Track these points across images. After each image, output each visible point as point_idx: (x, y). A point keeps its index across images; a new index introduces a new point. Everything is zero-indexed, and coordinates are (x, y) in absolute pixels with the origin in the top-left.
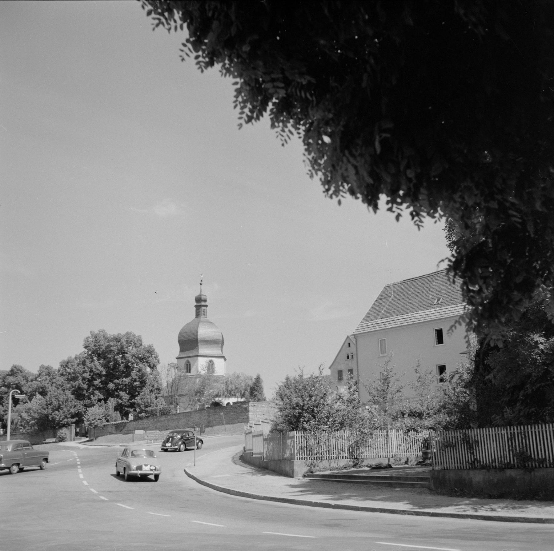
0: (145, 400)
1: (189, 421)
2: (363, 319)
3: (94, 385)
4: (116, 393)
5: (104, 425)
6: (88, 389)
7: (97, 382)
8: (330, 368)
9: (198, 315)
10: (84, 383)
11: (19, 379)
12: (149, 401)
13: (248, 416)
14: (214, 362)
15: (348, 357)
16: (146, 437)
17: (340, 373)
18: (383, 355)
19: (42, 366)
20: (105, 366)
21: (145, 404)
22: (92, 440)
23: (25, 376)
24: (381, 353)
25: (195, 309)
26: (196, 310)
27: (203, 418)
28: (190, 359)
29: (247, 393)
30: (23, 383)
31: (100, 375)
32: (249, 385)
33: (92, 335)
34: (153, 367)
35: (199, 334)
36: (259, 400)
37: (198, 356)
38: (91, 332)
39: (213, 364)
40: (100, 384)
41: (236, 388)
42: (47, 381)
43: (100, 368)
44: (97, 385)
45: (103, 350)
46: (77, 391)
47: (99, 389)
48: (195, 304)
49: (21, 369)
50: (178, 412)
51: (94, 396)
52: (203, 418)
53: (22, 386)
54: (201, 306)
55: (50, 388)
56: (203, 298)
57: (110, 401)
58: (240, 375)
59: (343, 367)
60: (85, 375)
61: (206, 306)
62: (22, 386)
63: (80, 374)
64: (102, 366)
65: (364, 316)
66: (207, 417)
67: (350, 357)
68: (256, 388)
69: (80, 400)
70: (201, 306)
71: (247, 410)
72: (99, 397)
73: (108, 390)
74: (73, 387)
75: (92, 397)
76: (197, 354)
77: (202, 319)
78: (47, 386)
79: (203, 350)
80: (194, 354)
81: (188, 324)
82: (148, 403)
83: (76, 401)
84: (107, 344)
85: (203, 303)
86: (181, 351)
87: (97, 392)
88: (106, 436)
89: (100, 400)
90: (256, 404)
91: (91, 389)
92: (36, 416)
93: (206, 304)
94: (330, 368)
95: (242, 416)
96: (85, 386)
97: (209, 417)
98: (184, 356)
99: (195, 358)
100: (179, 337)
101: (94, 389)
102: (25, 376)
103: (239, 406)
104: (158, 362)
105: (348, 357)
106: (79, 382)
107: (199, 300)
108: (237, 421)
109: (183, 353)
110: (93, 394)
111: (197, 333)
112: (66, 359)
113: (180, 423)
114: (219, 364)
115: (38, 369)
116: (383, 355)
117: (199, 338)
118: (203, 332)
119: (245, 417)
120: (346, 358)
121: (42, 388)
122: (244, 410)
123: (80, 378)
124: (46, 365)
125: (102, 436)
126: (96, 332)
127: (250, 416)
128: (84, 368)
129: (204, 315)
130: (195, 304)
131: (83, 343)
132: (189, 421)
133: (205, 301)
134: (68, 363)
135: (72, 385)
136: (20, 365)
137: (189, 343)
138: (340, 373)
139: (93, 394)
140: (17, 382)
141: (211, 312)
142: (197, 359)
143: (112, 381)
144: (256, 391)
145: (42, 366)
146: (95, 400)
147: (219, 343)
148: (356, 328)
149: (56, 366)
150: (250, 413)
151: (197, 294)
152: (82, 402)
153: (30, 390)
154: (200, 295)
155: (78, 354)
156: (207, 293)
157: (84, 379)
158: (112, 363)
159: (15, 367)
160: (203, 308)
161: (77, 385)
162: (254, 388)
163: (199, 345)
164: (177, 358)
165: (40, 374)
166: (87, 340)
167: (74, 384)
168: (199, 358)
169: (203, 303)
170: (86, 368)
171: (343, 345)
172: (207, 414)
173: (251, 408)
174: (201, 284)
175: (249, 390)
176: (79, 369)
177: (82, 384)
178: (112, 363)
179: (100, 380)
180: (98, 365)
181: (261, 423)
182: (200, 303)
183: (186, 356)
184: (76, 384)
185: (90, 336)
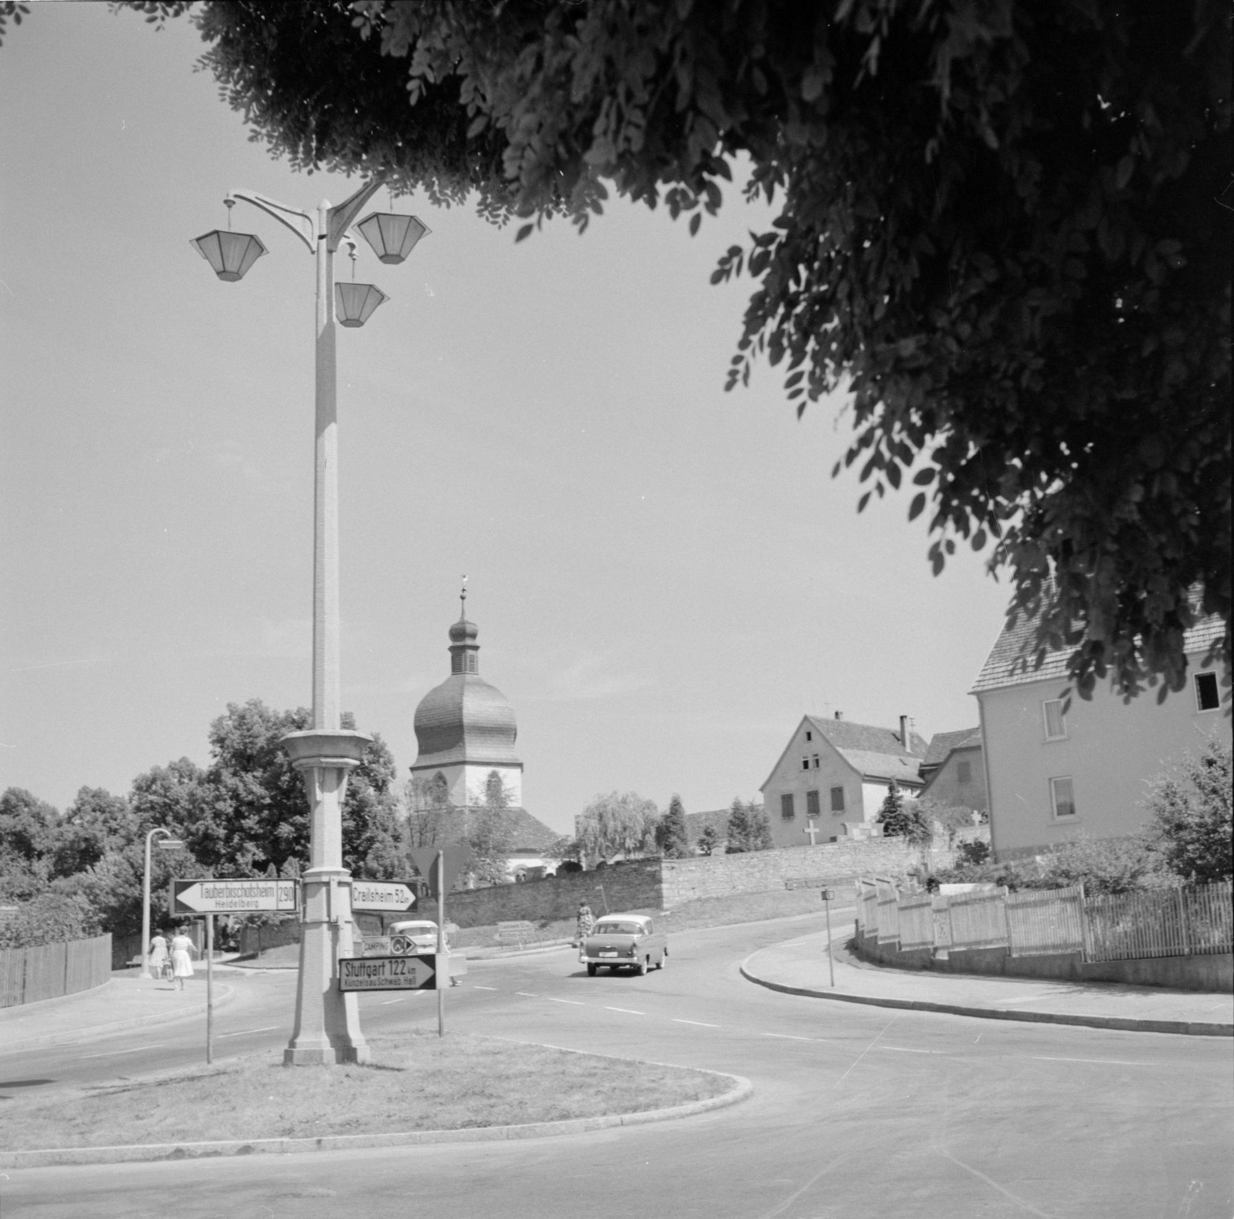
0: (388, 862)
1: (504, 906)
2: (991, 656)
3: (242, 829)
4: (298, 848)
5: (281, 922)
6: (228, 839)
7: (250, 822)
8: (762, 790)
9: (457, 667)
10: (218, 826)
11: (24, 820)
12: (396, 863)
13: (659, 891)
14: (501, 775)
15: (806, 764)
16: (497, 937)
17: (787, 800)
18: (1053, 738)
19: (85, 790)
20: (267, 784)
21: (385, 871)
22: (253, 957)
23: (39, 814)
24: (1051, 735)
25: (449, 654)
26: (453, 658)
27: (541, 899)
28: (444, 771)
29: (650, 839)
30: (34, 829)
31: (254, 806)
32: (653, 822)
33: (232, 713)
34: (380, 787)
35: (465, 711)
36: (681, 855)
37: (464, 763)
38: (229, 705)
39: (499, 781)
40: (256, 827)
41: (625, 829)
42: (99, 825)
43: (259, 790)
44: (251, 829)
45: (262, 748)
46: (199, 844)
47: (253, 837)
48: (450, 643)
49: (26, 798)
50: (471, 886)
51: (243, 855)
52: (541, 899)
53: (33, 836)
54: (464, 648)
55: (106, 840)
56: (469, 629)
57: (290, 864)
58: (631, 799)
59: (797, 785)
60: (220, 805)
61: (476, 648)
62: (33, 836)
63: (207, 803)
64: (261, 784)
65: (991, 648)
66: (551, 896)
67: (811, 764)
68: (673, 828)
69: (206, 864)
70: (464, 648)
71: (656, 879)
72: (256, 858)
73: (277, 840)
74: (192, 834)
75: (238, 856)
76: (461, 759)
77: (469, 677)
78: (99, 835)
79: (474, 748)
80: (454, 759)
81: (436, 690)
82: (393, 867)
83: (198, 866)
84: (269, 734)
85: (469, 642)
86: (423, 751)
87: (250, 845)
88: (286, 947)
89: (256, 864)
90: (676, 863)
91: (236, 839)
92: (113, 902)
93: (477, 642)
94: (762, 790)
95: (644, 892)
96: (222, 832)
97: (558, 896)
98: (429, 763)
99: (458, 767)
100: (417, 718)
101: (241, 839)
102: (39, 814)
103: (635, 870)
104: (393, 774)
105: (806, 764)
106: (207, 823)
107: (459, 634)
108: (631, 906)
109: (428, 756)
110: (241, 849)
111: (461, 709)
112: (148, 772)
113: (481, 912)
114: (511, 779)
115: (75, 796)
116: (1053, 738)
117: (466, 721)
118: (475, 708)
119: (653, 894)
120: (802, 766)
121: (86, 840)
122: (648, 879)
123: (208, 814)
124: (94, 787)
125: (274, 946)
126: (242, 705)
127: (665, 893)
128: (218, 789)
129: (472, 669)
130: (450, 643)
131: (209, 729)
132: (504, 906)
133: (474, 636)
134: (154, 781)
135: (187, 829)
136: (23, 788)
137: (441, 733)
138: (787, 800)
139: (241, 849)
140: (19, 828)
141: (486, 657)
142: (462, 771)
143: (285, 820)
144: (674, 834)
145: (85, 790)
146: (247, 864)
147: (505, 732)
148: (979, 678)
149: (121, 789)
150: (664, 886)
151: (454, 620)
152: (212, 869)
153: (58, 844)
154: (463, 622)
155: (176, 760)
156: (474, 619)
157: (217, 815)
158: (286, 778)
159: (12, 792)
160: (470, 652)
161: (202, 828)
162: (667, 828)
163: (467, 737)
164: (412, 769)
165: (79, 809)
166: (218, 724)
167: (193, 828)
168: (468, 768)
169: (469, 642)
170: (223, 790)
171: (794, 737)
172: (551, 890)
173: (665, 874)
174: (463, 598)
175: (654, 833)
176: (206, 792)
177: (214, 826)
178: (286, 778)
179: (257, 818)
180: (253, 784)
181: (874, 882)
182: (462, 642)
183: (434, 763)
184: (200, 826)
185: (227, 714)
